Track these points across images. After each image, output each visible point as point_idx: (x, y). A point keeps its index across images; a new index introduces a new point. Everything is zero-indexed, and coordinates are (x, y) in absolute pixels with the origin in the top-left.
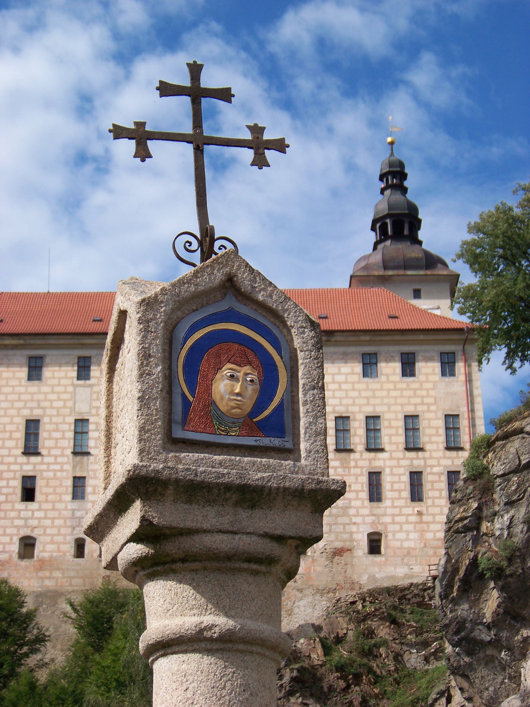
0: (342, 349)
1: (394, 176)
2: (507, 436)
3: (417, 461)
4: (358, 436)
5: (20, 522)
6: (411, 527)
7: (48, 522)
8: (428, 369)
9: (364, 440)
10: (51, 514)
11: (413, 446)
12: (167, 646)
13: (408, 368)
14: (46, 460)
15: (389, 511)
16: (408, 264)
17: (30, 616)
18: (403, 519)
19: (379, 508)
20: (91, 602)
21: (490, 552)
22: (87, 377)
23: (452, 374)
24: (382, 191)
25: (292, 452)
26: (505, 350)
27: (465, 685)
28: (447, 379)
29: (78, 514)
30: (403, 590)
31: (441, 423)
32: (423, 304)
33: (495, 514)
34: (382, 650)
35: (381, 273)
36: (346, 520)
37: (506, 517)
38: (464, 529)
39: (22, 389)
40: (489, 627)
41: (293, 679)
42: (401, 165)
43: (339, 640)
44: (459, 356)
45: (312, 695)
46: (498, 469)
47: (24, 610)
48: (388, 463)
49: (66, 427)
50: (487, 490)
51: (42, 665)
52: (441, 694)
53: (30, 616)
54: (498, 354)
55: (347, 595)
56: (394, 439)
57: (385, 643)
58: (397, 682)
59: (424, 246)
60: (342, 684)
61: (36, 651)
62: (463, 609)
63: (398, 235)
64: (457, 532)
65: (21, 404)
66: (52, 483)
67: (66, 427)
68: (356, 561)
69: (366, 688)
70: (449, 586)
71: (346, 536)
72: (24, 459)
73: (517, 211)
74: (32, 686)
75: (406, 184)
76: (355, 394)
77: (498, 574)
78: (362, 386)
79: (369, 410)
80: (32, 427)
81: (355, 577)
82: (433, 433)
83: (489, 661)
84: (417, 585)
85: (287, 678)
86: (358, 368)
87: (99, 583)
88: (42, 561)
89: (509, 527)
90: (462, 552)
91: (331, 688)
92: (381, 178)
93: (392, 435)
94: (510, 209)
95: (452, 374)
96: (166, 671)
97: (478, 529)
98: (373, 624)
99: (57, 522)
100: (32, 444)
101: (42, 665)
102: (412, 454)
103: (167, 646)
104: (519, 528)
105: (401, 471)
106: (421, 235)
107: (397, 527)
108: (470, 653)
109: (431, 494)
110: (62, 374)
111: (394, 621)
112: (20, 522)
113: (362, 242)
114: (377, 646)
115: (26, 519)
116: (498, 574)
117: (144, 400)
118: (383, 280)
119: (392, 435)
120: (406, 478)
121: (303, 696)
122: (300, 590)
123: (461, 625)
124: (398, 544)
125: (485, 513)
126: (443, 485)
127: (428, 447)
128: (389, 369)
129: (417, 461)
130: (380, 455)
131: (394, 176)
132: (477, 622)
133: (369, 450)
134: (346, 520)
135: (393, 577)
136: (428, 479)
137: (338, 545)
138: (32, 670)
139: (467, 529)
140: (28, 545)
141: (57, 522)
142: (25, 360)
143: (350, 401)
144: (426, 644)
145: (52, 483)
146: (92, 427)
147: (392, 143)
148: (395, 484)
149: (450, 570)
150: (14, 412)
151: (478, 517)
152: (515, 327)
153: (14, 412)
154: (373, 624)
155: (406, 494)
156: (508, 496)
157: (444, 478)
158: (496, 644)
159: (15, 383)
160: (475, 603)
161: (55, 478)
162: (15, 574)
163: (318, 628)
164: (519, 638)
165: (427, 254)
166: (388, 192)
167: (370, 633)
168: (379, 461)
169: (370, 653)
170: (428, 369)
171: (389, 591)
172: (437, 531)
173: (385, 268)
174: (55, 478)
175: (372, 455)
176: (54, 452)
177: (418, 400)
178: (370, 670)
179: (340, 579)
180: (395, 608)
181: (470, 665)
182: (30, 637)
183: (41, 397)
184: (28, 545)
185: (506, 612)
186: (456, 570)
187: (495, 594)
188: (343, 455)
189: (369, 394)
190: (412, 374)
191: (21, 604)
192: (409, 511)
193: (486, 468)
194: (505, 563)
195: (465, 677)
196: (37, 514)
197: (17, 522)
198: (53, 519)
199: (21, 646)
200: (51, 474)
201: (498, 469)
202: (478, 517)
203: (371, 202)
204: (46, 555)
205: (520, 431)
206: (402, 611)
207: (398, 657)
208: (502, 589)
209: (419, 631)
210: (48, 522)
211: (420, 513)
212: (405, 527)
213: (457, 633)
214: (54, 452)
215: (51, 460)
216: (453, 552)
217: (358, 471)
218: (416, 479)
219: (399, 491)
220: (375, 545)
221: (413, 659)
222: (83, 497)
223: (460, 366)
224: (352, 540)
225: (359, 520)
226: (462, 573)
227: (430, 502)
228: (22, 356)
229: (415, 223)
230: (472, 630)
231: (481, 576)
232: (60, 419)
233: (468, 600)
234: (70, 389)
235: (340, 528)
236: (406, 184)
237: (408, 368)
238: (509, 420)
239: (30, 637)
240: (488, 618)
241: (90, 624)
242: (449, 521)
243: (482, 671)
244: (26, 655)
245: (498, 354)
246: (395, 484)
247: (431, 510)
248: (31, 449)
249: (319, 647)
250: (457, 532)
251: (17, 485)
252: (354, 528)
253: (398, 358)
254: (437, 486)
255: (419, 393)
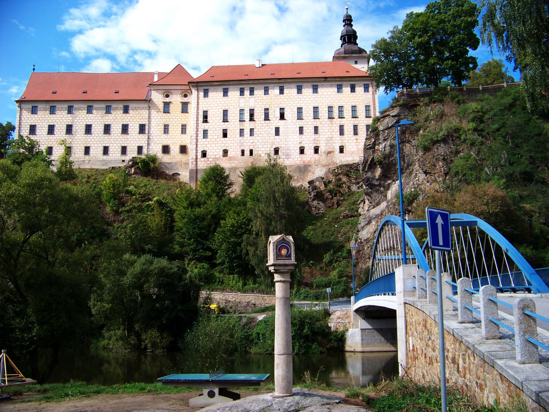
0: (330, 83)
1: (348, 20)
2: (384, 117)
3: (355, 121)
4: (336, 113)
5: (223, 145)
6: (354, 144)
7: (232, 145)
8: (360, 90)
9: (338, 114)
10: (233, 142)
11: (354, 117)
12: (277, 282)
13: (353, 90)
14: (231, 123)
15: (347, 139)
16: (353, 52)
17: (228, 176)
18: (351, 141)
19: (343, 137)
20: (247, 172)
21: (378, 156)
22: (243, 95)
23: (368, 91)
24: (344, 26)
25: (291, 259)
26: (384, 87)
27: (370, 198)
28: (366, 93)
29: (242, 141)
30: (351, 165)
31: (364, 108)
32: (358, 66)
33: (380, 143)
34: (344, 185)
35: (344, 55)
36: (332, 142)
37: (384, 144)
38: (370, 148)
39: (221, 100)
40: (377, 180)
41: (314, 195)
42: (351, 16)
43: (330, 182)
44: (370, 85)
45: (321, 200)
46: (381, 128)
47: (226, 174)
48: (346, 122)
49: (237, 112)
50: (377, 135)
51: (232, 192)
52: (362, 201)
53: (228, 176)
54: (382, 88)
55: (332, 167)
56: (348, 114)
57: (345, 183)
58: (349, 196)
59: (359, 46)
60: (331, 196)
61: (229, 188)
62: (369, 175)
63: (349, 42)
64: (368, 149)
65: (221, 105)
66: (233, 131)
67: (237, 112)
68: (335, 155)
69: (338, 198)
70: (364, 167)
71: (332, 147)
72: (223, 123)
73: (388, 40)
74: (230, 200)
75: (352, 23)
76: (335, 99)
77: (380, 163)
78: (337, 96)
79: (340, 105)
80: (225, 113)
81: (335, 161)
82: (361, 112)
83: (377, 191)
84: (356, 163)
85: (312, 195)
86: (336, 90)
87: (250, 165)
88: (230, 158)
89: (384, 148)
90: (369, 156)
91: (327, 198)
92: (344, 21)
93: (347, 113)
94: (386, 40)
95: (368, 91)
96: (277, 284)
97: (374, 148)
98: (341, 176)
99: (235, 144)
100: (225, 118)
101: (232, 192)
102: (354, 119)
103: (277, 282)
104: (388, 148)
105: (351, 125)
106: (358, 41)
107: (349, 144)
108: (371, 188)
109: (360, 133)
110: (235, 94)
111: (348, 176)
112: (223, 145)
113: (337, 44)
114: (342, 184)
115: (225, 144)
116: (380, 163)
117: (274, 249)
118: (344, 58)
119: (347, 113)
120: (352, 127)
121: (318, 201)
122: (317, 166)
123: (368, 179)
124: (349, 150)
125: (377, 143)
126: (365, 129)
127: (359, 117)
128: (347, 90)
129: (355, 121)
130: (343, 119)
131: (348, 20)
132: (373, 178)
133: (339, 118)
134: (332, 142)
135: (348, 161)
136: (359, 128)
137: (329, 150)
138: (229, 194)
139: (370, 148)
140: (225, 152)
141: (235, 144)
142: (222, 90)
143: (333, 101)
144: (358, 183)
145: (233, 131)
146: (245, 112)
147: (347, 9)
148: (348, 130)
149: (365, 161)
150: (219, 108)
151: (374, 144)
152: (388, 80)
153: (219, 108)
154: (341, 176)
155: (352, 133)
156: (384, 137)
157: (365, 127)
158: (380, 185)
159: (219, 97)
160: (373, 172)
161: (234, 130)
162: (222, 162)
163: (323, 178)
164: (387, 183)
165: (359, 48)
166: (346, 26)
167: (340, 180)
168: (343, 122)
169: (340, 186)
170: (360, 90)
171: (346, 166)
172: (361, 146)
173: (345, 53)
174: (234, 130)
175: (341, 119)
176: (233, 121)
177: (356, 101)
178: (340, 192)
179: (330, 161)
180: (348, 171)
181: (371, 192)
182: (228, 183)
183: (228, 102)
184: (225, 152)
185: (383, 175)
186: (367, 162)
187: (379, 169)
188: (331, 119)
189: (340, 98)
190: (354, 92)
191: (224, 173)
192: (353, 138)
193: (377, 128)
194: (383, 160)
195: (370, 196)
196: (228, 142)
197: (222, 145)
198: (233, 143)
199: (225, 186)
200: (232, 128)
201: (381, 128)
202: (374, 144)
203: (340, 29)
204: (232, 155)
205: (389, 115)
206: (351, 172)
207: (349, 187)
208: (382, 168)
209: (356, 179)
210: (232, 145)
211: (357, 139)
212: (352, 144)
213: (367, 182)
214: (233, 121)
215: (232, 123)
216: (366, 156)
217: (336, 125)
218: (355, 128)
219: (350, 132)
220: (342, 150)
221: (354, 188)
222: (243, 136)
223: (370, 89)
224: (334, 149)
225: (336, 142)
226: (369, 163)
227: (360, 135)
228: (221, 88)
229: (356, 37)
230: (372, 181)
231: (375, 164)
232: (235, 110)
233: (371, 171)
234: (238, 99)
235: (330, 145)
236: (352, 23)
237: (353, 90)
238: (385, 112)
239: (228, 183)
240: (377, 177)
241: (247, 179)
242: (365, 145)
243: (375, 194)
244: (227, 189)
245: (382, 88)
246: (348, 130)
247: (361, 138)
248: (225, 120)
249: (323, 184)
250: (368, 149)
251: (221, 132)
252: (335, 145)
253: (349, 86)
254: (362, 130)
255: (357, 98)
